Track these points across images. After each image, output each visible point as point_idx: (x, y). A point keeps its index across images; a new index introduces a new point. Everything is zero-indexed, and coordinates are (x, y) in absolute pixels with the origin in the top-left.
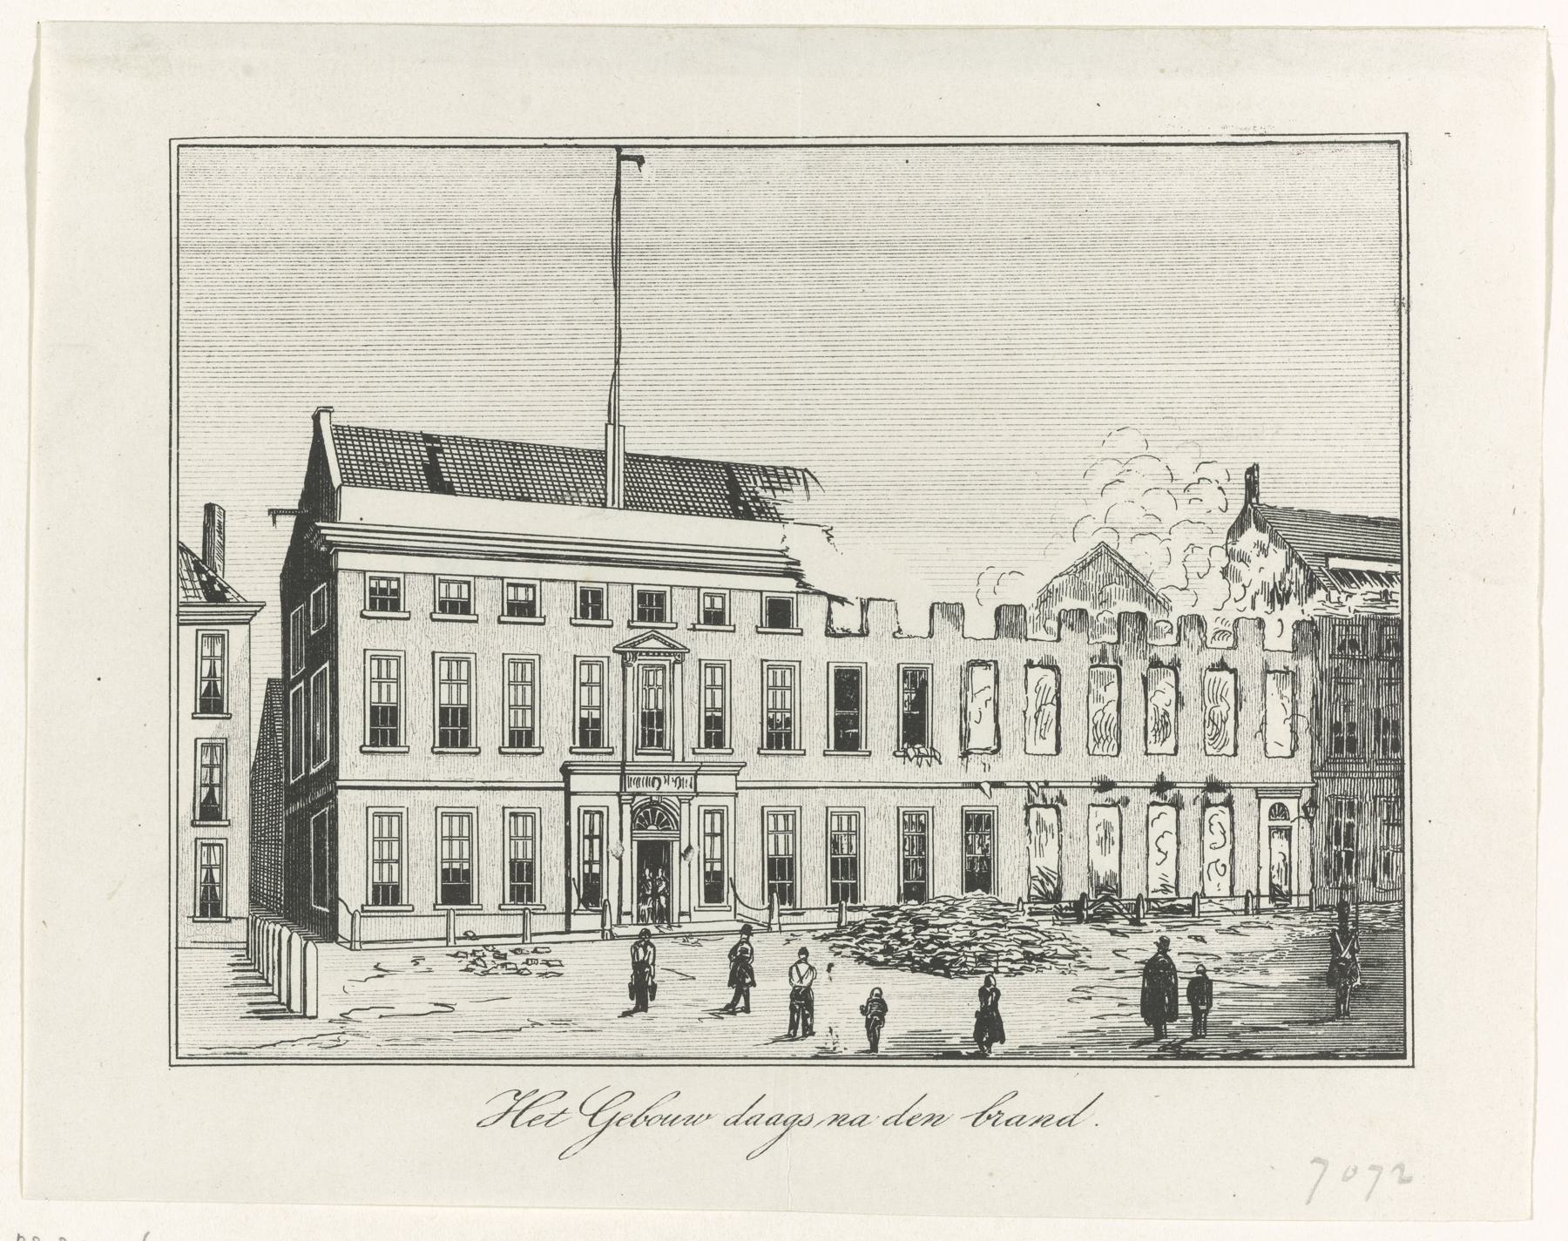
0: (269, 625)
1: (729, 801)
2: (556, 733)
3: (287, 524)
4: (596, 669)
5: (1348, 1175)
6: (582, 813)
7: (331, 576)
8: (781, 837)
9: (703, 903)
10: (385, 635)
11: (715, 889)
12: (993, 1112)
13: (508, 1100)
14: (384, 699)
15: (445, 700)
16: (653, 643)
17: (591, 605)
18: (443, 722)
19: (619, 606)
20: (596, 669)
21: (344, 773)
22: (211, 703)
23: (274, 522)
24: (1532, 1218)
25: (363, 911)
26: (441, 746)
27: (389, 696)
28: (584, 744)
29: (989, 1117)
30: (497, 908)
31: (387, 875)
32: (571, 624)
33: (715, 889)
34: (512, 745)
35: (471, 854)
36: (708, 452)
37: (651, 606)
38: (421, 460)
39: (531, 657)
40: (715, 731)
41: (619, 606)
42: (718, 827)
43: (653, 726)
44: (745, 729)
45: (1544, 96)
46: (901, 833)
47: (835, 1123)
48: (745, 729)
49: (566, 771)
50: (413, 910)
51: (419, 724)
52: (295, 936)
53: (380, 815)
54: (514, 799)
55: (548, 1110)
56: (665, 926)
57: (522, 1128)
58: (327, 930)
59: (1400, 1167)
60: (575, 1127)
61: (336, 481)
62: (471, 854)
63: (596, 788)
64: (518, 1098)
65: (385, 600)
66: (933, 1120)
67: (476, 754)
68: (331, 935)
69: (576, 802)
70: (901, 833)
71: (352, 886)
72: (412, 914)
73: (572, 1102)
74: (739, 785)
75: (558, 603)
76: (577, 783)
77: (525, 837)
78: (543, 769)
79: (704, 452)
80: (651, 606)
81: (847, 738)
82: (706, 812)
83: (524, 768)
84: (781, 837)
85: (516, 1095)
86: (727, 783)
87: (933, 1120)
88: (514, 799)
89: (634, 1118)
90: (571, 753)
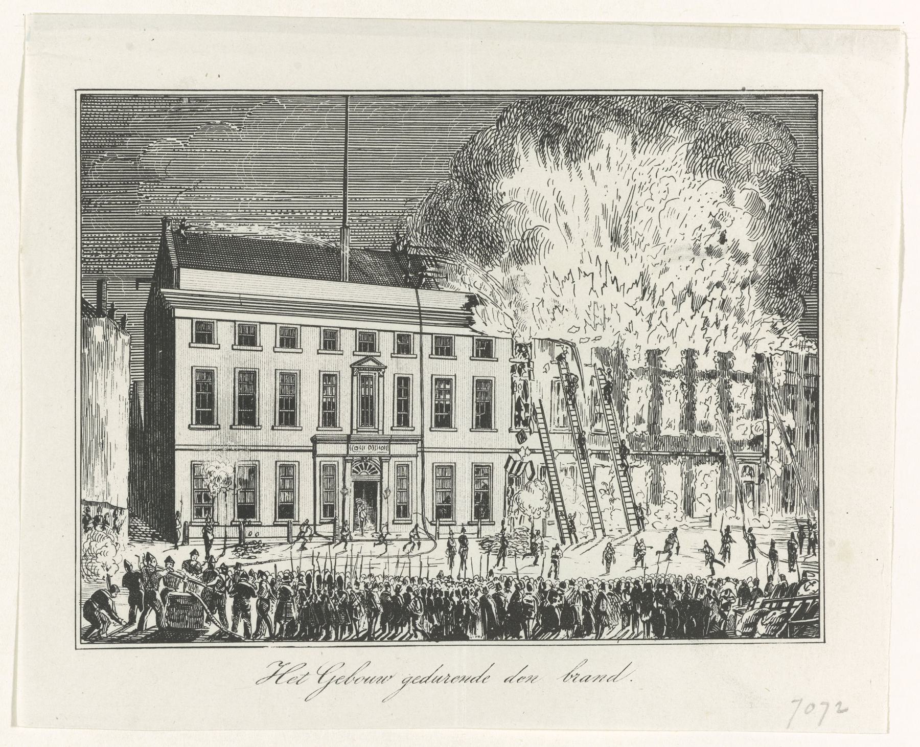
3: (145, 288)
5: (808, 710)
10: (205, 357)
11: (402, 511)
12: (574, 674)
13: (276, 667)
16: (371, 363)
17: (330, 342)
19: (347, 341)
23: (137, 287)
24: (888, 732)
29: (572, 676)
33: (402, 511)
37: (367, 343)
41: (347, 341)
46: (475, 400)
47: (530, 681)
49: (315, 440)
54: (284, 456)
55: (298, 674)
56: (358, 532)
59: (839, 703)
60: (311, 684)
61: (174, 261)
66: (532, 679)
69: (318, 460)
70: (475, 400)
73: (312, 668)
75: (310, 339)
78: (302, 438)
80: (367, 343)
81: (484, 420)
83: (287, 437)
87: (532, 679)
88: (284, 456)
89: (347, 677)
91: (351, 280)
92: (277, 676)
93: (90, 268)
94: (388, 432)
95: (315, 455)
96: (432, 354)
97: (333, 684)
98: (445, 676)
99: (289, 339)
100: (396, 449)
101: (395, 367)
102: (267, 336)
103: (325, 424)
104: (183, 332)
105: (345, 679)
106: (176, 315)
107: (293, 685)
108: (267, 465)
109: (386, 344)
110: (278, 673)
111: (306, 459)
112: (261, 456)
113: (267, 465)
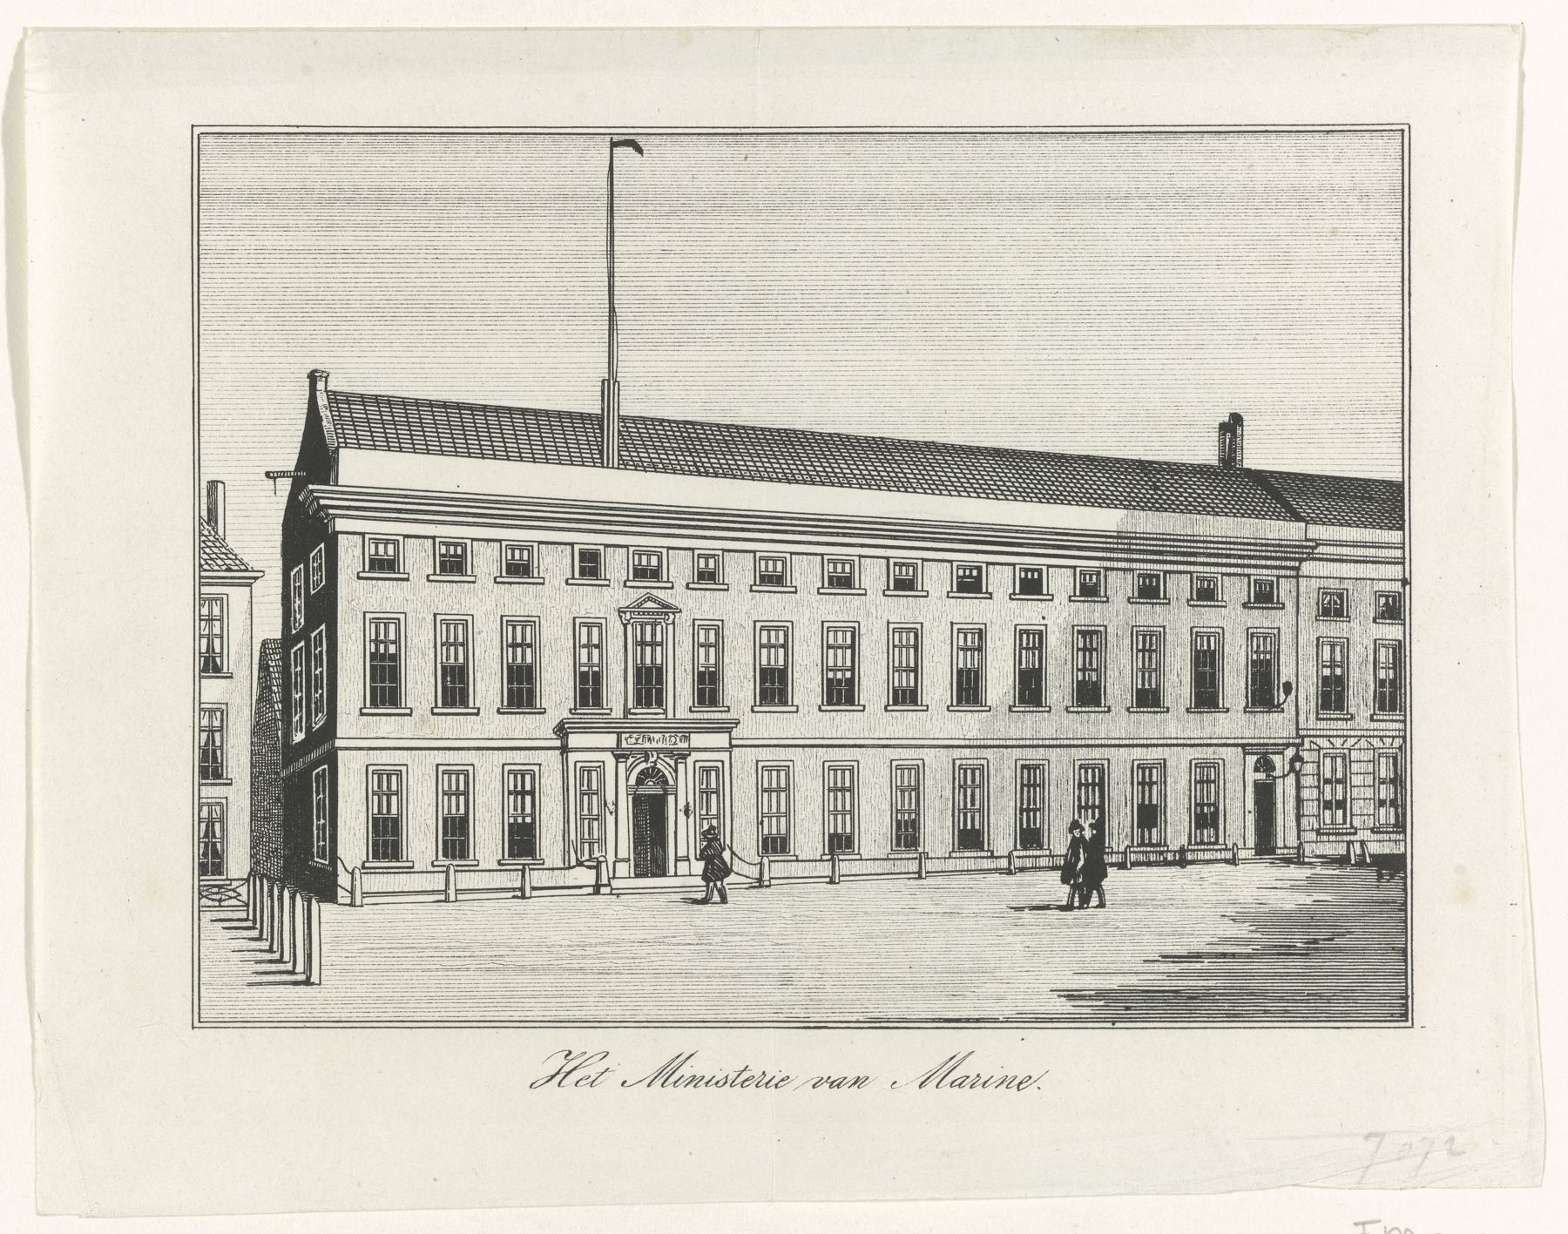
0: (270, 589)
1: (725, 756)
2: (556, 688)
3: (285, 485)
4: (595, 631)
6: (370, 772)
7: (332, 541)
8: (969, 782)
9: (894, 848)
10: (383, 596)
13: (559, 1061)
14: (773, 663)
15: (961, 665)
17: (590, 565)
18: (763, 681)
20: (595, 631)
21: (342, 729)
22: (210, 665)
25: (363, 867)
26: (445, 704)
27: (456, 657)
28: (701, 701)
30: (496, 863)
31: (773, 828)
32: (884, 595)
34: (894, 704)
35: (852, 805)
36: (1334, 468)
38: (953, 457)
39: (598, 621)
40: (708, 687)
42: (712, 785)
43: (649, 685)
44: (739, 687)
45: (1512, 210)
48: (739, 687)
50: (543, 864)
51: (806, 684)
52: (298, 897)
53: (449, 773)
55: (592, 1070)
57: (669, 1088)
58: (327, 891)
62: (852, 805)
63: (592, 744)
64: (569, 1058)
65: (383, 566)
67: (542, 713)
68: (329, 894)
71: (353, 842)
72: (476, 868)
74: (734, 742)
76: (574, 740)
77: (1029, 786)
79: (1318, 468)
81: (1206, 696)
82: (1081, 767)
83: (522, 726)
84: (969, 782)
85: (567, 1056)
86: (721, 740)
90: (691, 711)
91: (624, 465)
92: (558, 1077)
93: (1376, 508)
94: (683, 713)
95: (564, 750)
96: (888, 589)
97: (732, 1076)
98: (758, 1073)
99: (453, 564)
100: (697, 740)
101: (695, 605)
102: (485, 561)
103: (701, 701)
104: (350, 556)
105: (591, 1080)
106: (337, 529)
107: (585, 1089)
108: (1179, 764)
109: (680, 568)
110: (563, 1070)
111: (551, 760)
112: (929, 756)
113: (1179, 764)
